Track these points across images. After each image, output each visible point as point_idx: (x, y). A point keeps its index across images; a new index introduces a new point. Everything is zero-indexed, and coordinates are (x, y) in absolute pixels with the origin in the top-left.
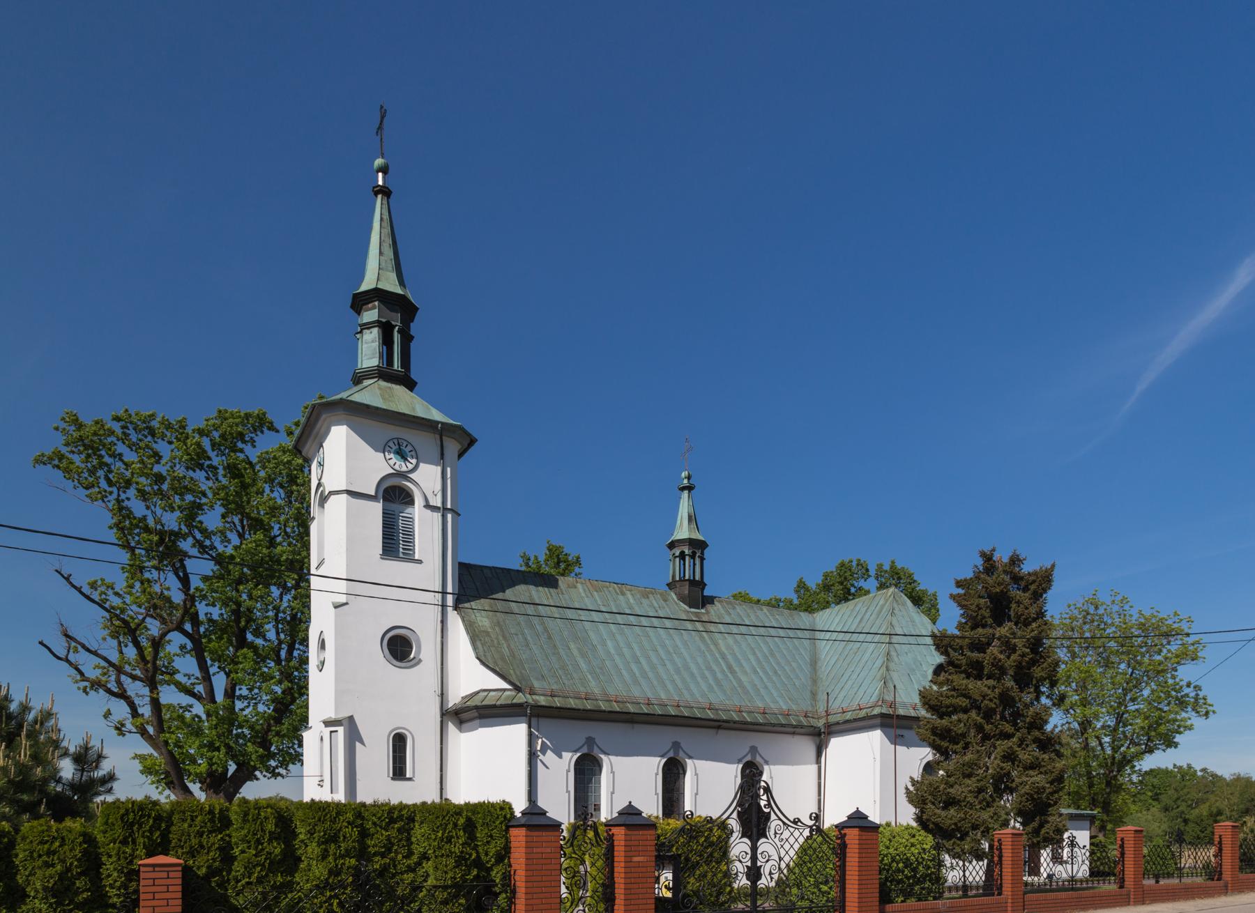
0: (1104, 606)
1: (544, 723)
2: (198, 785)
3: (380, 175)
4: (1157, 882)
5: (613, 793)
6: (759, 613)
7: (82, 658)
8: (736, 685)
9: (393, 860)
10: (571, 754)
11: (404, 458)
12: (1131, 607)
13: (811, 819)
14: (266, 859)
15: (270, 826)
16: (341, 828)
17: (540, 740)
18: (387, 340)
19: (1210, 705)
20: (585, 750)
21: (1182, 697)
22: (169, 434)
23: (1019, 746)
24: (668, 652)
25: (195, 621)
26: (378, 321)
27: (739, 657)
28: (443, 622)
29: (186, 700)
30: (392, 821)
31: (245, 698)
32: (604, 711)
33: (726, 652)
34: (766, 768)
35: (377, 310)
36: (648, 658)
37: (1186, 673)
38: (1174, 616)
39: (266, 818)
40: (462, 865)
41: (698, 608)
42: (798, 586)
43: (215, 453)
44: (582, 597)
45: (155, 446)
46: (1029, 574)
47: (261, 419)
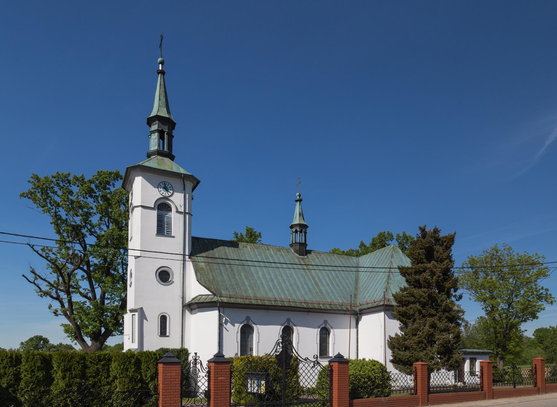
0: (501, 252)
1: (227, 310)
2: (89, 338)
3: (160, 65)
4: (515, 387)
5: (258, 342)
6: (332, 257)
7: (39, 282)
8: (318, 292)
9: (99, 379)
10: (239, 325)
11: (167, 190)
12: (513, 251)
13: (314, 358)
14: (36, 379)
15: (39, 364)
16: (73, 364)
17: (224, 318)
18: (161, 137)
19: (553, 298)
20: (245, 323)
21: (540, 294)
22: (77, 183)
23: (439, 320)
24: (287, 277)
25: (89, 266)
26: (157, 130)
27: (321, 278)
28: (184, 264)
29: (84, 299)
30: (100, 361)
31: (109, 299)
32: (254, 305)
33: (315, 276)
34: (332, 330)
35: (157, 125)
36: (277, 279)
37: (542, 283)
38: (536, 255)
39: (37, 360)
40: (133, 381)
41: (304, 256)
42: (361, 245)
43: (97, 190)
44: (249, 252)
45: (70, 188)
46: (443, 237)
47: (117, 175)
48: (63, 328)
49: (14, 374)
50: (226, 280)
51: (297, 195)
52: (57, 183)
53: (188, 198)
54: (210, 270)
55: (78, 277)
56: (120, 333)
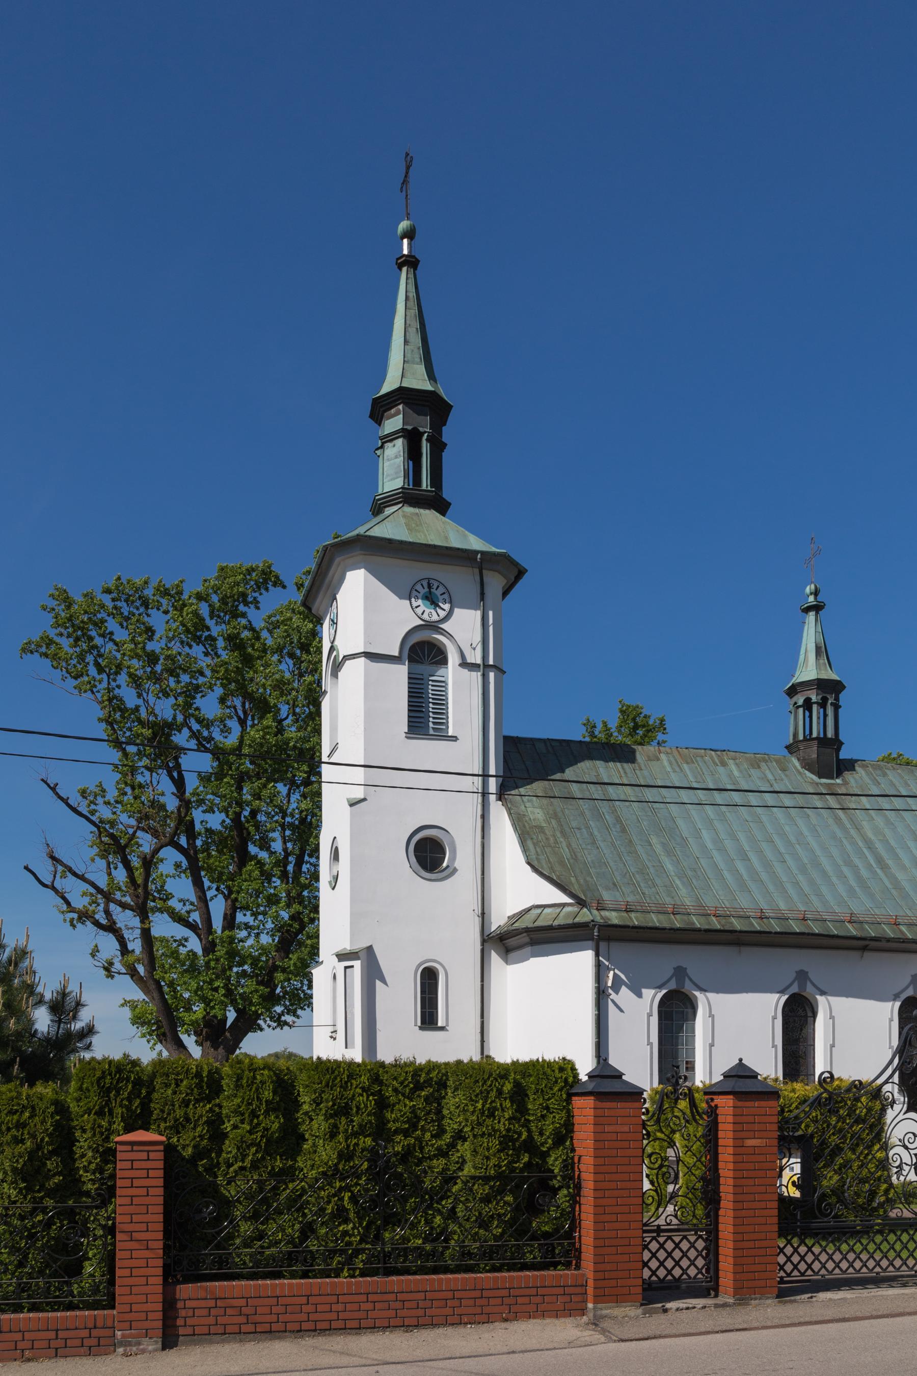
2: (193, 1038)
8: (889, 886)
11: (434, 604)
14: (262, 1136)
15: (267, 1094)
16: (354, 1096)
17: (612, 973)
18: (413, 454)
20: (673, 985)
25: (192, 834)
26: (403, 430)
28: (484, 817)
30: (418, 1087)
32: (699, 930)
33: (873, 838)
35: (401, 416)
36: (760, 853)
41: (832, 778)
43: (214, 621)
44: (668, 773)
48: (127, 1013)
49: (209, 1123)
50: (610, 861)
51: (808, 590)
52: (115, 608)
53: (493, 624)
54: (562, 832)
55: (166, 868)
56: (275, 1024)
